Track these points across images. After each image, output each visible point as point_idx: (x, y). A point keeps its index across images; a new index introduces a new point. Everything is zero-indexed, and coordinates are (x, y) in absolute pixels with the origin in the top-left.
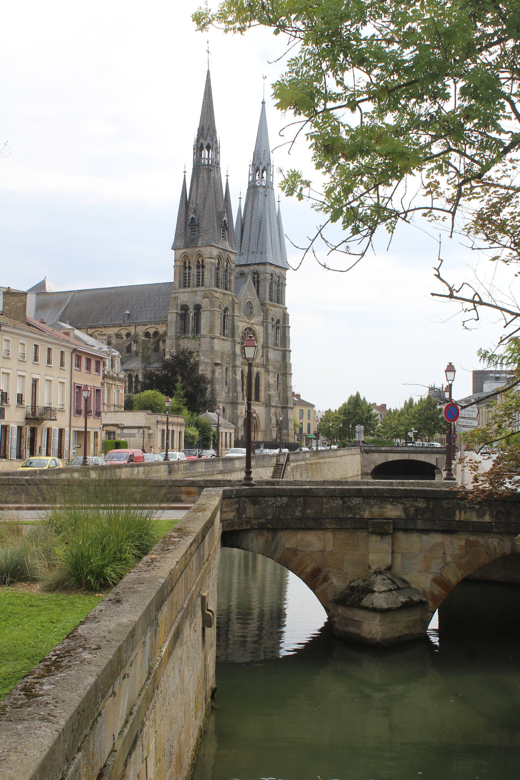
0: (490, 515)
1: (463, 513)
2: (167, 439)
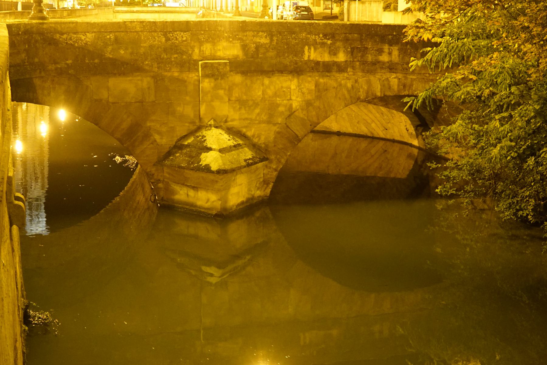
0: (344, 51)
1: (312, 49)
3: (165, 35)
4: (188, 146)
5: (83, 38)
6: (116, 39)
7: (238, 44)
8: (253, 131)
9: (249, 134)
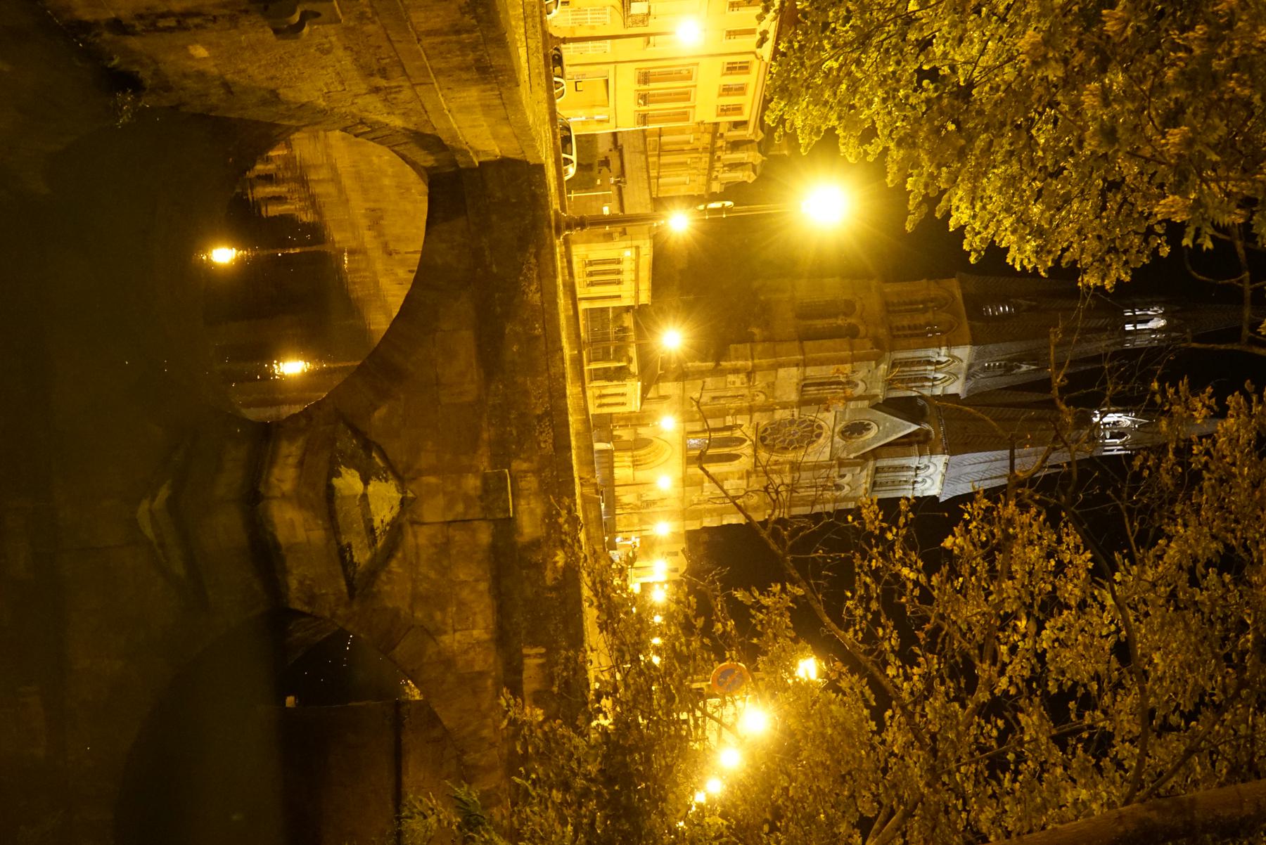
2: (604, 273)
3: (547, 413)
4: (370, 456)
5: (533, 288)
6: (537, 338)
7: (540, 532)
8: (400, 570)
9: (394, 565)
